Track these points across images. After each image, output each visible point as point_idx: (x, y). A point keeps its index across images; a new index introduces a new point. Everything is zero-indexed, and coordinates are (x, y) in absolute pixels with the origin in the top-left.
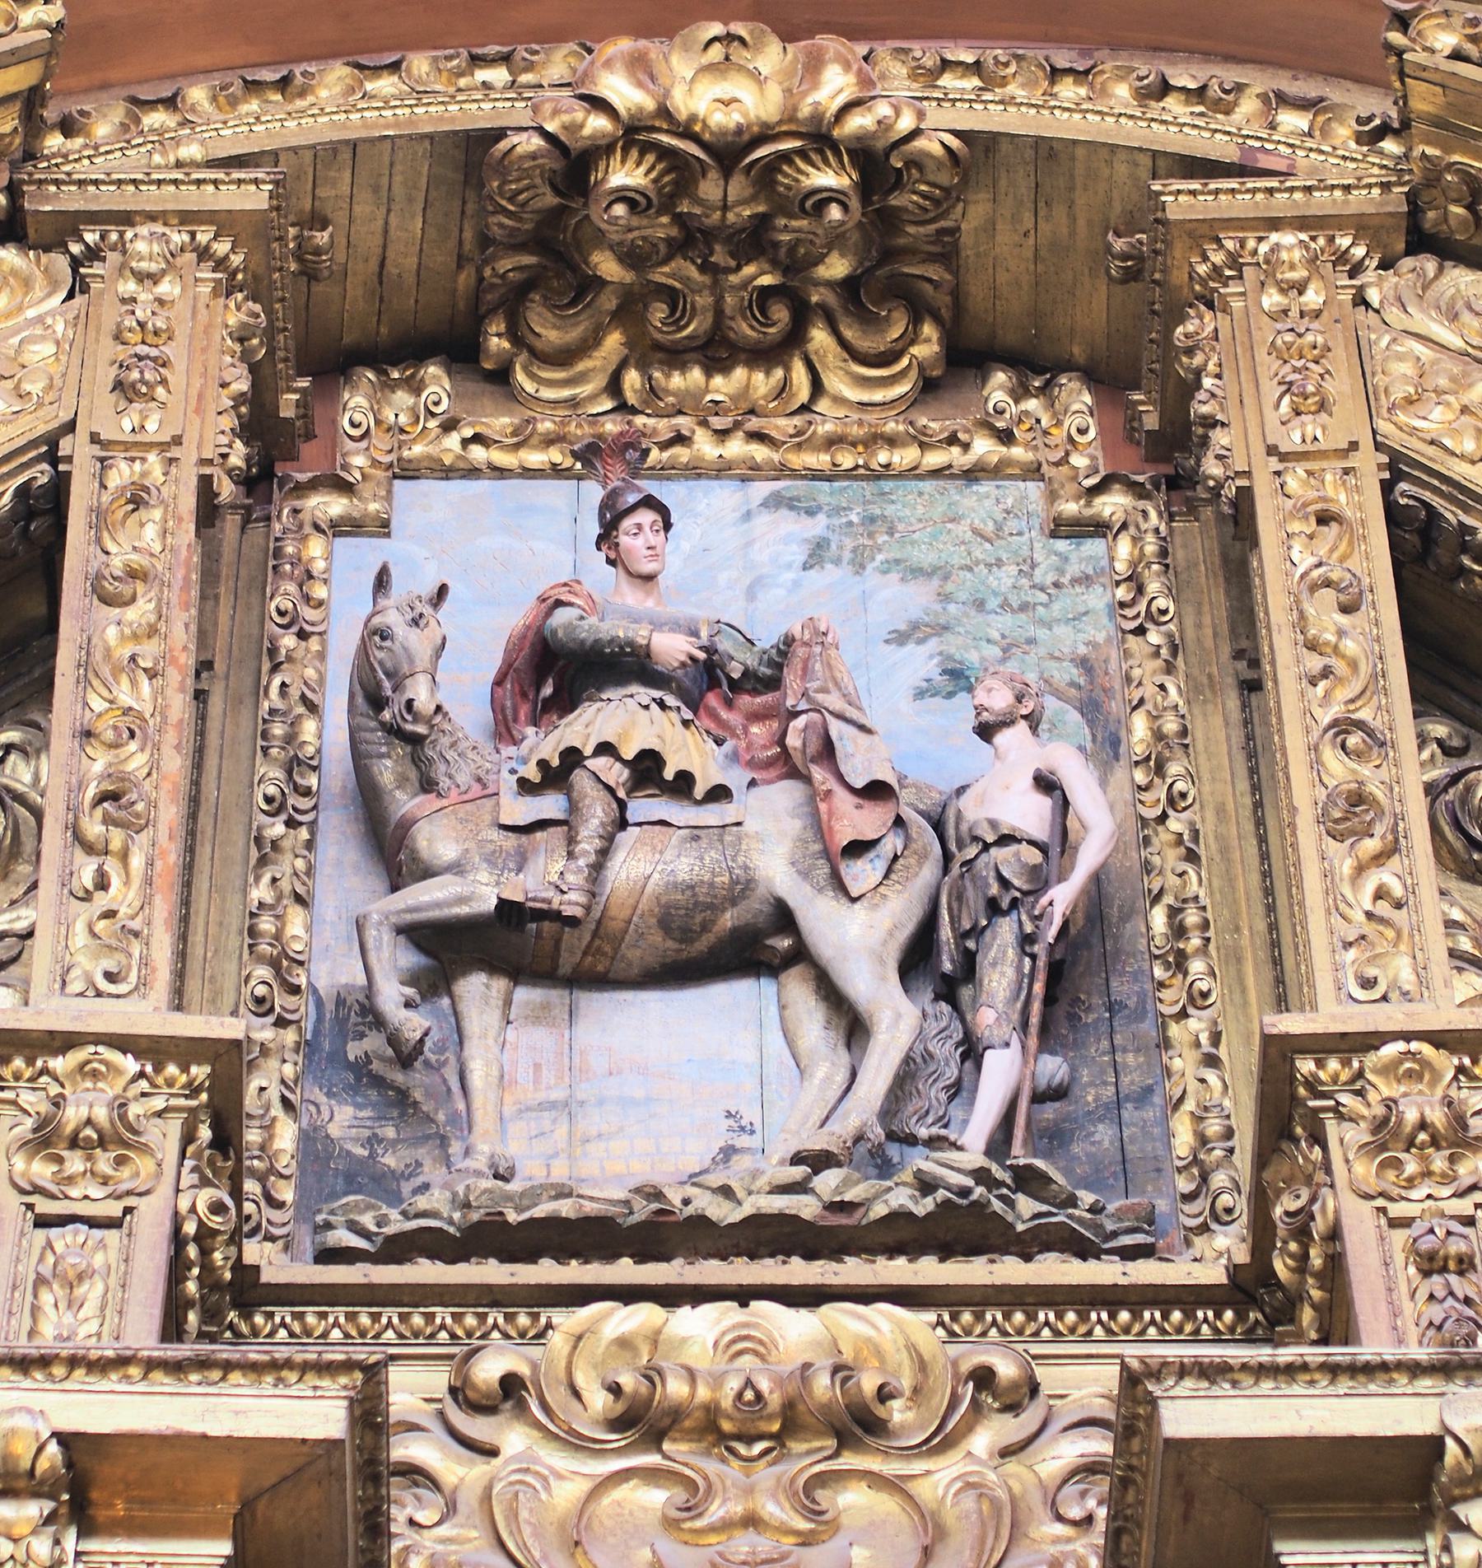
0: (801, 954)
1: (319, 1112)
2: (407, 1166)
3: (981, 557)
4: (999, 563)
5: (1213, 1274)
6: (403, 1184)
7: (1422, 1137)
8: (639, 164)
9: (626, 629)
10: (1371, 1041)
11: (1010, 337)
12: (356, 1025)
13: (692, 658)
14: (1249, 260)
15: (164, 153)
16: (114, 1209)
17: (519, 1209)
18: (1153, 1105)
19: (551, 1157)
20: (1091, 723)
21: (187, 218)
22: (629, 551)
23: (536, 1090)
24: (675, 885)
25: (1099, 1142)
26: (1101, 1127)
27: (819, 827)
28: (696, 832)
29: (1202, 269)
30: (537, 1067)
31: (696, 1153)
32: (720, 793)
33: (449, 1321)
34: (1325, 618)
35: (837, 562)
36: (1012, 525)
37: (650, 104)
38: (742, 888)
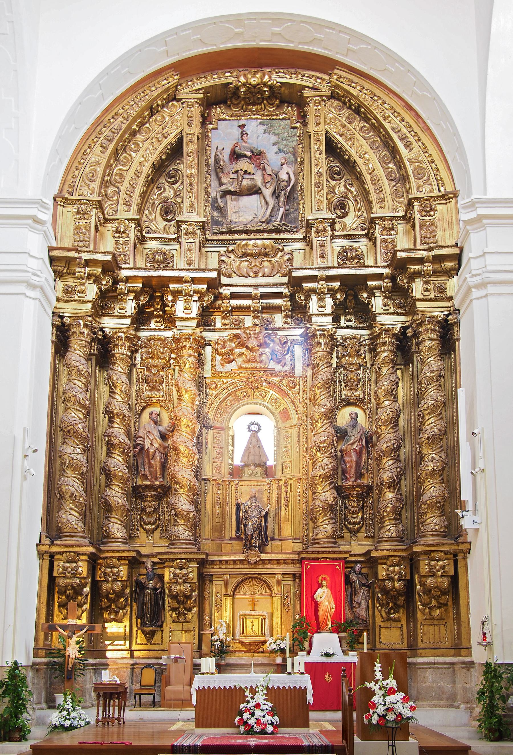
0: (261, 193)
5: (302, 237)
10: (317, 219)
11: (287, 100)
16: (193, 241)
27: (264, 179)
28: (251, 180)
32: (253, 174)
34: (317, 155)
38: (255, 186)
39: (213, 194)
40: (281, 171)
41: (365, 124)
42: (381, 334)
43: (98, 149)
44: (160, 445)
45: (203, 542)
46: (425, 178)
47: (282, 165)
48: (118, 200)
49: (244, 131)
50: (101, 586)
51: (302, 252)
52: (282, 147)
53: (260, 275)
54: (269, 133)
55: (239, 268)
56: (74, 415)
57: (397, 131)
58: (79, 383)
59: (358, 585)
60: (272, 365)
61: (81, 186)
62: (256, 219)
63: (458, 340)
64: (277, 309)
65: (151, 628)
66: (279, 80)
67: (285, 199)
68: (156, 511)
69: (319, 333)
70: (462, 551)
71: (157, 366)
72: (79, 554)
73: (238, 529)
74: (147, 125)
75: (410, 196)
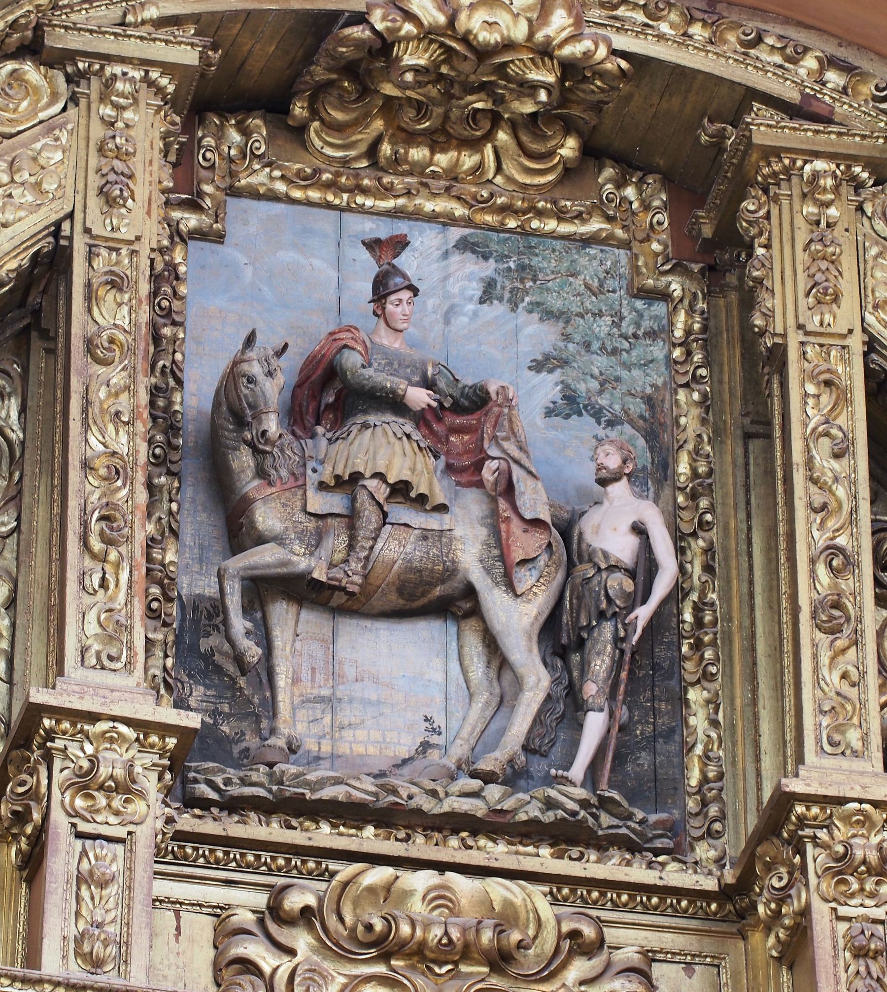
1: (183, 688)
2: (236, 734)
3: (590, 307)
4: (600, 314)
5: (710, 884)
6: (234, 746)
7: (863, 868)
8: (426, 51)
9: (392, 382)
10: (842, 801)
12: (205, 626)
13: (429, 405)
14: (796, 172)
15: (135, 14)
16: (121, 832)
17: (313, 791)
18: (674, 742)
19: (321, 737)
20: (652, 449)
21: (146, 63)
22: (392, 314)
23: (312, 687)
24: (411, 569)
25: (643, 765)
26: (643, 754)
28: (425, 535)
29: (766, 171)
30: (313, 670)
31: (405, 746)
33: (269, 860)
34: (822, 451)
35: (500, 299)
36: (610, 284)
37: (442, 19)
38: (451, 571)
47: (603, 482)
49: (395, 271)
52: (585, 387)
54: (514, 307)
62: (434, 755)
66: (621, 42)
67: (617, 665)
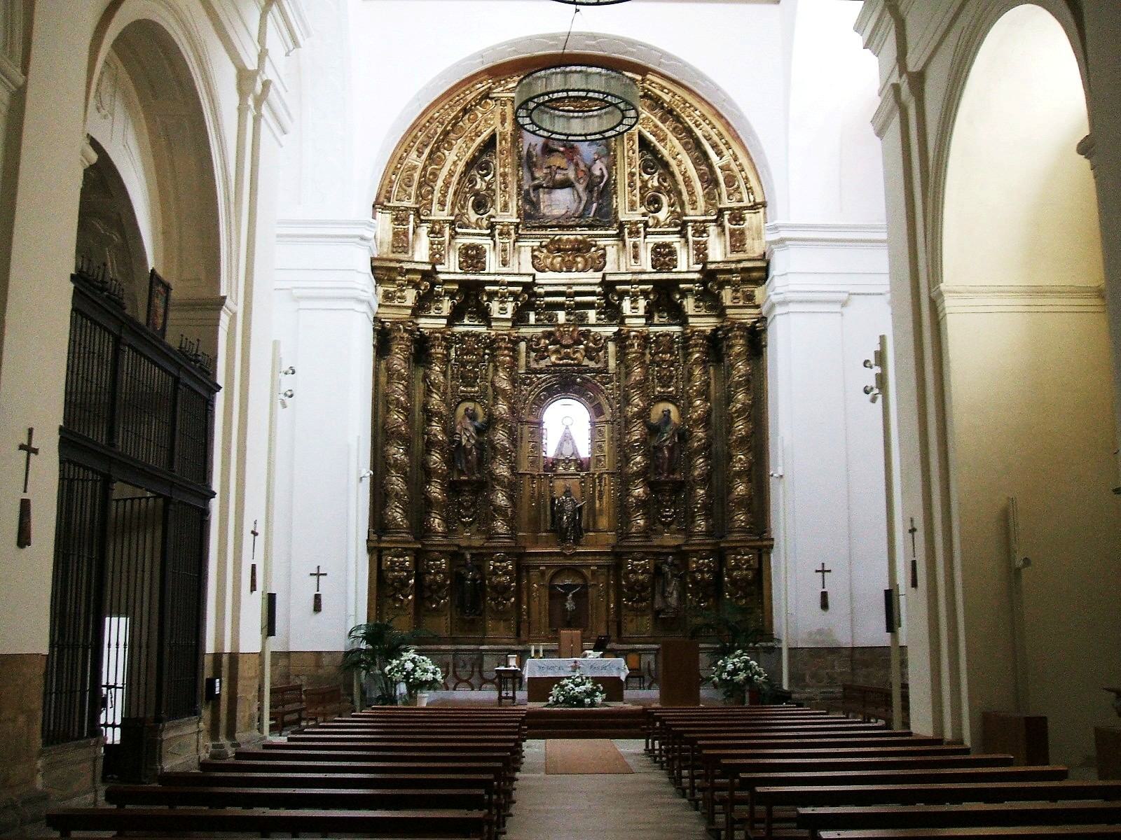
5: (615, 232)
28: (564, 175)
39: (526, 187)
40: (594, 166)
41: (678, 124)
42: (693, 335)
43: (414, 154)
44: (476, 441)
45: (520, 534)
46: (736, 186)
48: (432, 200)
50: (424, 578)
51: (615, 247)
53: (574, 270)
55: (552, 264)
56: (396, 417)
57: (708, 138)
58: (401, 386)
59: (670, 576)
60: (586, 362)
61: (398, 192)
63: (766, 346)
64: (590, 306)
65: (471, 617)
68: (473, 504)
69: (633, 333)
70: (766, 546)
71: (471, 362)
72: (405, 549)
73: (553, 522)
74: (461, 123)
75: (721, 206)
